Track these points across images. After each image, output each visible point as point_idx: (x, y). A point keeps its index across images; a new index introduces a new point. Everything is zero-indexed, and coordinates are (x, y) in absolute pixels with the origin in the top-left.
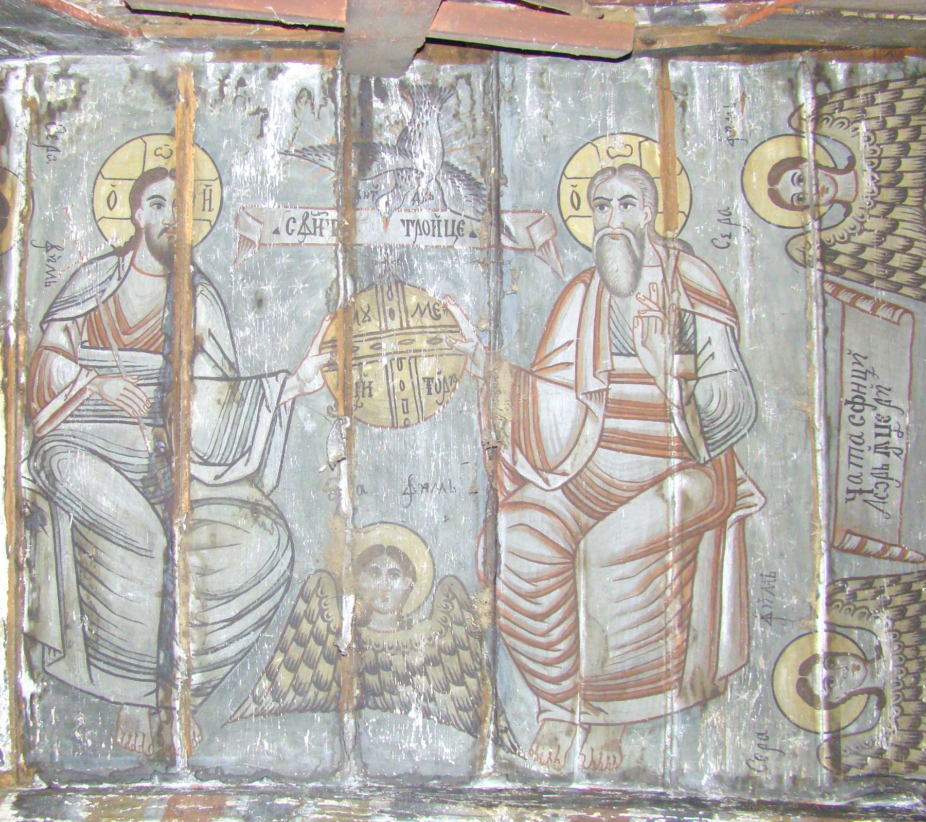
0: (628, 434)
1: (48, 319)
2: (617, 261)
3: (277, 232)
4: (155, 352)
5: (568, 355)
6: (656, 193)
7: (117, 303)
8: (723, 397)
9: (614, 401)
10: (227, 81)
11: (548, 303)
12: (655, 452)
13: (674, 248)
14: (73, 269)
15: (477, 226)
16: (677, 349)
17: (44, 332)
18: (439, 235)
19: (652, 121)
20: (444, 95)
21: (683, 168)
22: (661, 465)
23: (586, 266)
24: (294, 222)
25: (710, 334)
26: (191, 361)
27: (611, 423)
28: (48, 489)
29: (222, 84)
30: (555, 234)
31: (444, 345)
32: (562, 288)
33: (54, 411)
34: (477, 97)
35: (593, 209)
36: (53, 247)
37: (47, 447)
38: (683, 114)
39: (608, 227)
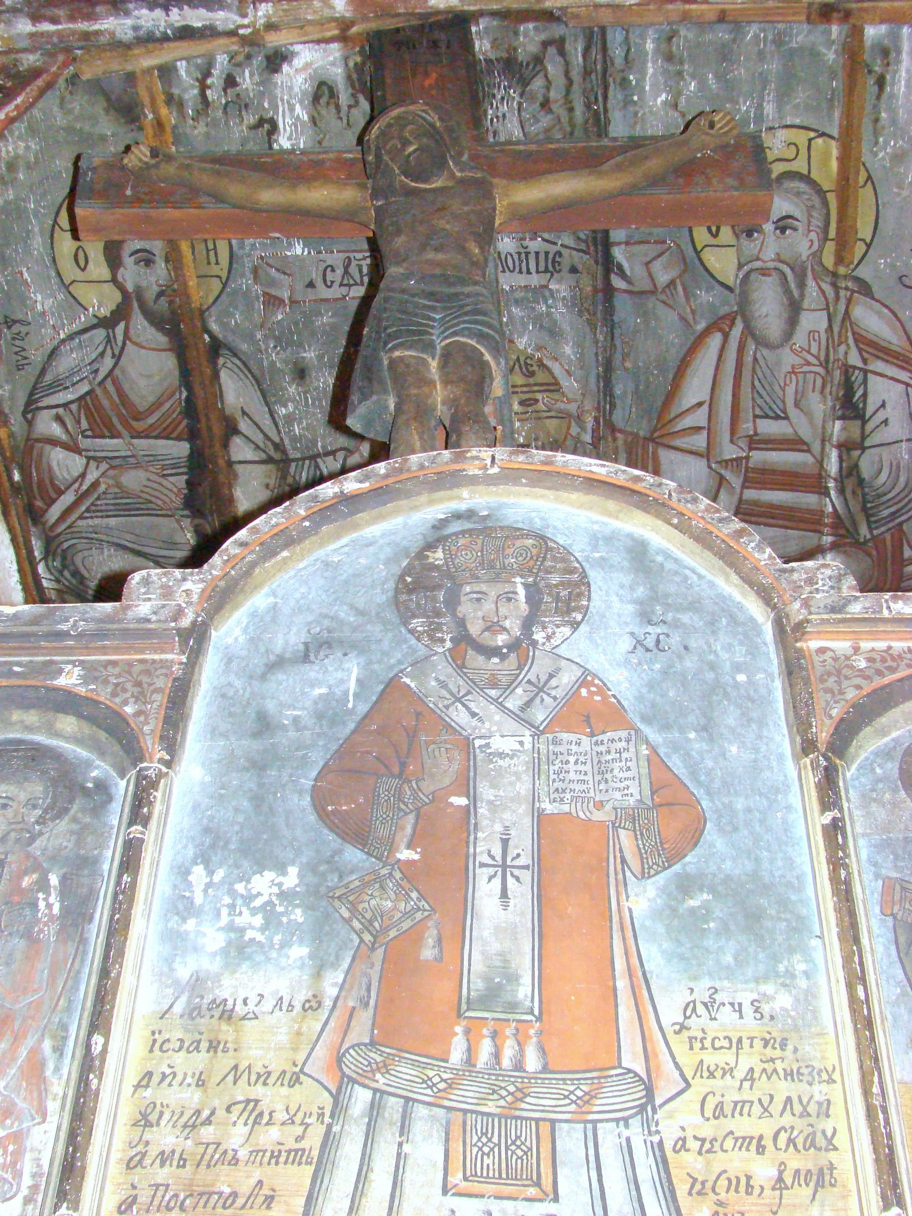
0: (772, 506)
1: (31, 408)
2: (768, 304)
3: (311, 285)
4: (179, 439)
5: (700, 418)
6: (828, 214)
7: (116, 383)
8: (896, 469)
9: (754, 470)
10: (209, 81)
11: (673, 357)
12: (803, 526)
13: (847, 289)
14: (50, 347)
15: (578, 259)
16: (840, 413)
17: (30, 423)
18: (529, 272)
19: (831, 108)
20: (527, 73)
21: (869, 178)
23: (725, 310)
24: (333, 270)
25: (885, 396)
26: (226, 445)
27: (751, 494)
29: (203, 87)
30: (685, 271)
31: (541, 407)
32: (692, 339)
33: (64, 508)
34: (575, 74)
35: (737, 237)
36: (15, 322)
37: (66, 545)
38: (878, 97)
39: (758, 259)
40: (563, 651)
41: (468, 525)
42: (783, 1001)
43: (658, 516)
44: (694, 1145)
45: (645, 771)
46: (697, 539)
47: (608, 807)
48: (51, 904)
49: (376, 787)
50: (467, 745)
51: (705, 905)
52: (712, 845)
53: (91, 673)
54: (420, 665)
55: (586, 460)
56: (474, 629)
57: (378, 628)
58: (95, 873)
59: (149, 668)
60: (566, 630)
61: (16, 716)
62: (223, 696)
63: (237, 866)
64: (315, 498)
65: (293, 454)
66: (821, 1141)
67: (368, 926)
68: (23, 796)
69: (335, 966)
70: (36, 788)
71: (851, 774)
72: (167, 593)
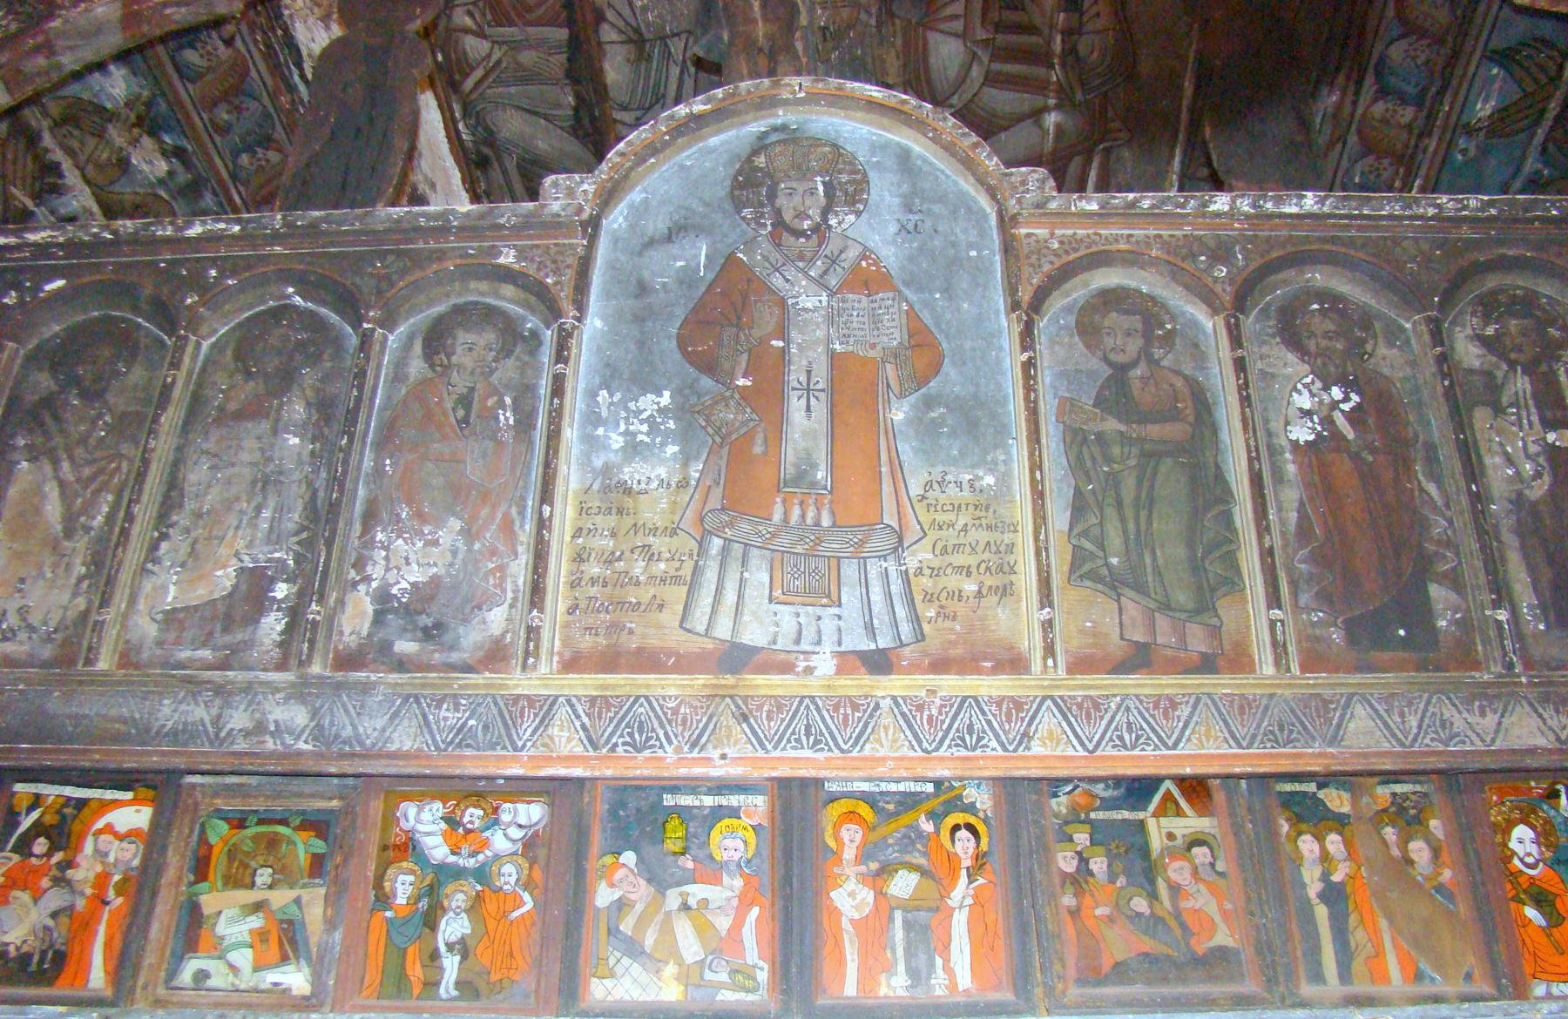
4: (560, 26)
22: (1039, 102)
26: (596, 31)
28: (490, 139)
40: (848, 233)
41: (781, 136)
42: (989, 480)
43: (918, 130)
44: (927, 572)
45: (904, 321)
46: (946, 149)
47: (879, 347)
48: (507, 417)
49: (718, 335)
50: (782, 303)
51: (942, 416)
52: (947, 374)
53: (522, 254)
54: (750, 244)
55: (868, 87)
56: (788, 217)
57: (720, 215)
58: (535, 397)
59: (562, 250)
60: (852, 218)
61: (473, 285)
62: (613, 268)
63: (629, 390)
64: (672, 117)
65: (647, 36)
66: (1006, 568)
67: (718, 431)
68: (482, 342)
69: (697, 458)
70: (490, 336)
71: (1042, 324)
72: (571, 193)
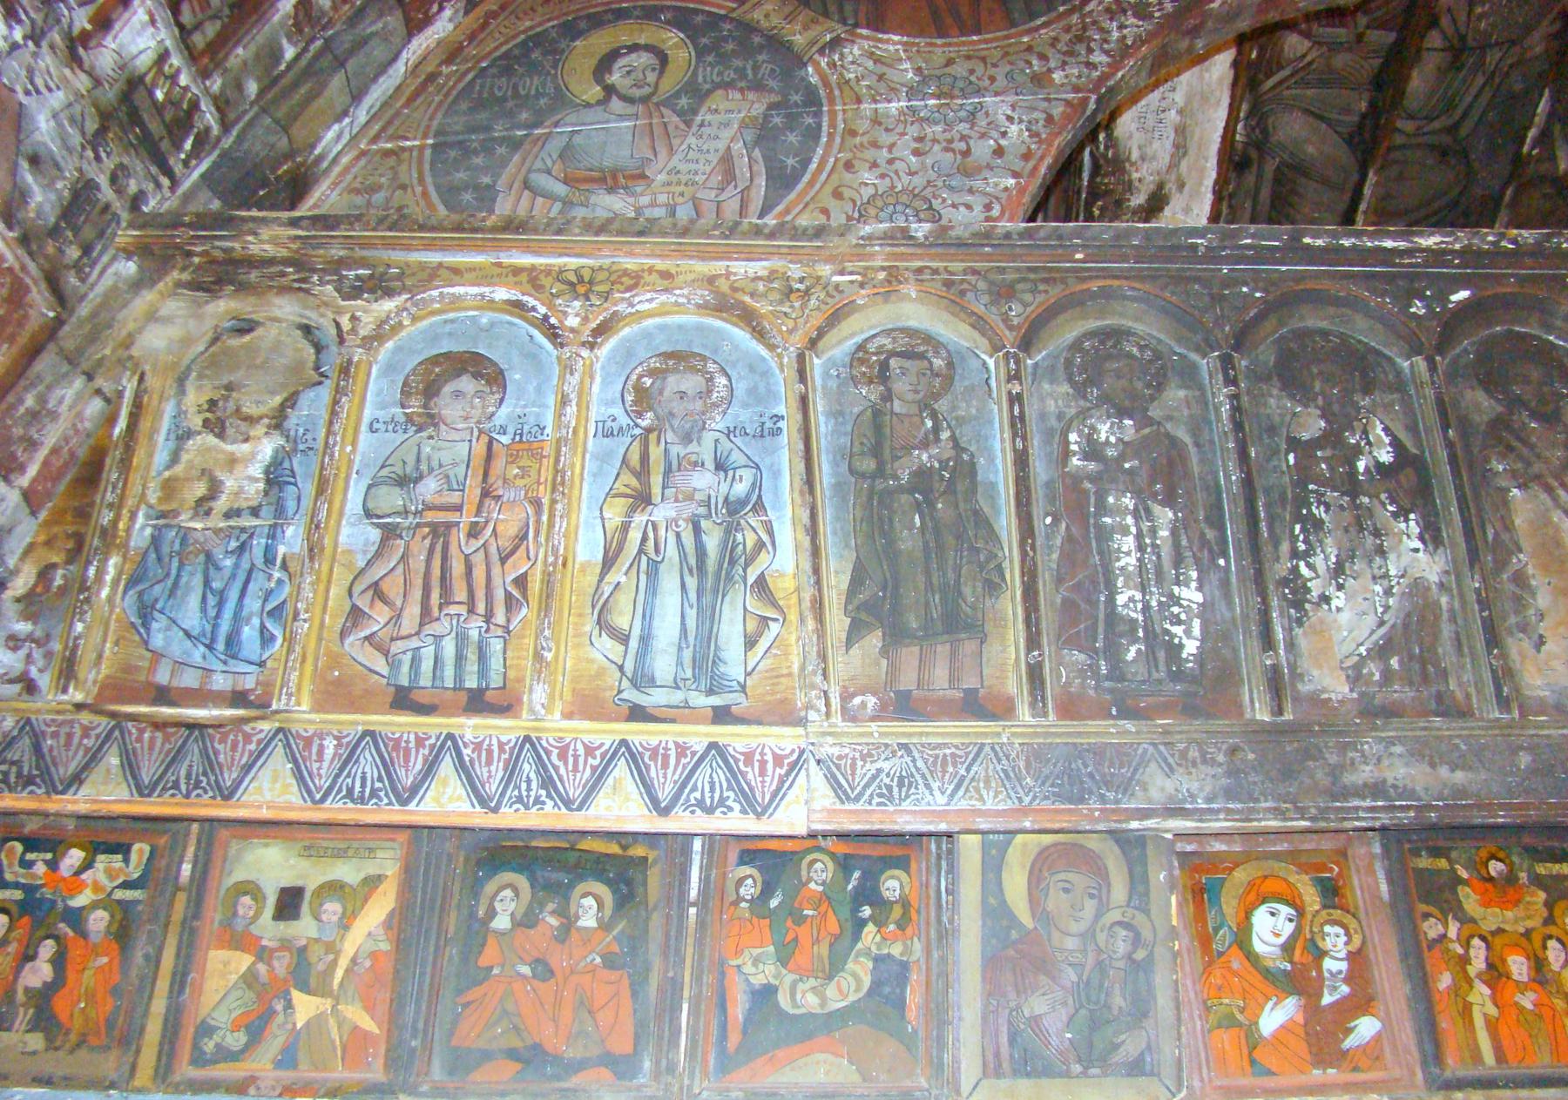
21: (383, 467)
65: (1471, 43)
